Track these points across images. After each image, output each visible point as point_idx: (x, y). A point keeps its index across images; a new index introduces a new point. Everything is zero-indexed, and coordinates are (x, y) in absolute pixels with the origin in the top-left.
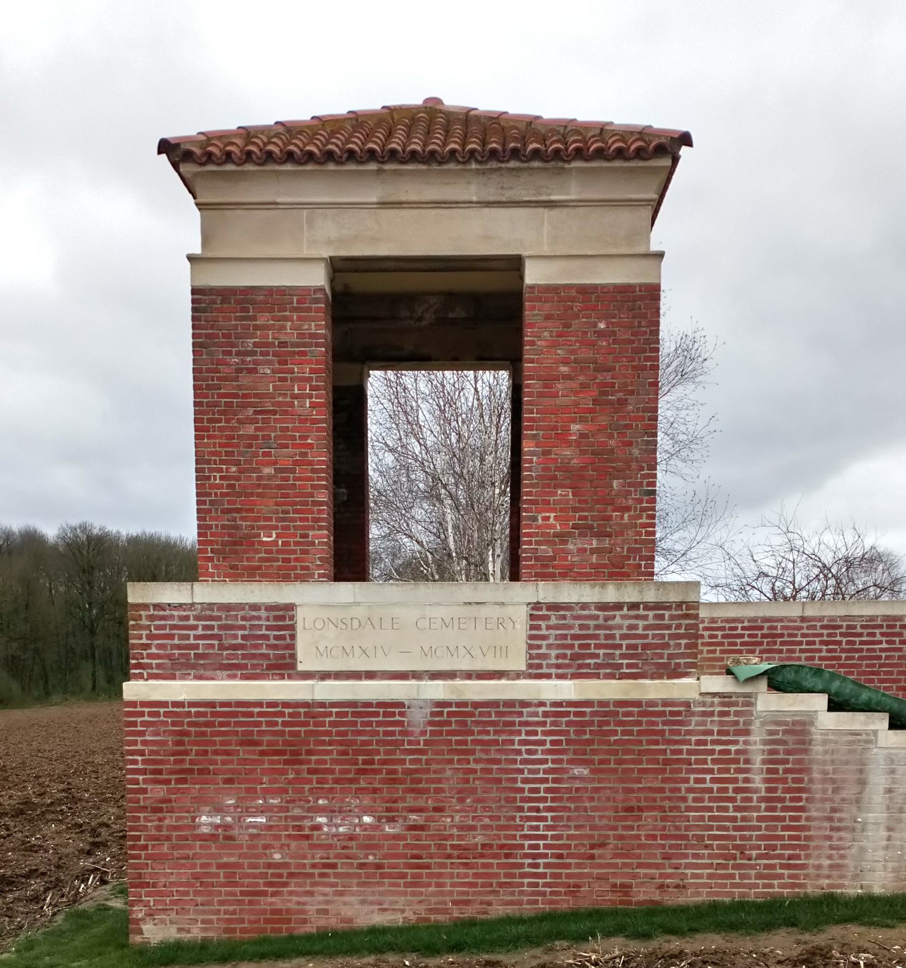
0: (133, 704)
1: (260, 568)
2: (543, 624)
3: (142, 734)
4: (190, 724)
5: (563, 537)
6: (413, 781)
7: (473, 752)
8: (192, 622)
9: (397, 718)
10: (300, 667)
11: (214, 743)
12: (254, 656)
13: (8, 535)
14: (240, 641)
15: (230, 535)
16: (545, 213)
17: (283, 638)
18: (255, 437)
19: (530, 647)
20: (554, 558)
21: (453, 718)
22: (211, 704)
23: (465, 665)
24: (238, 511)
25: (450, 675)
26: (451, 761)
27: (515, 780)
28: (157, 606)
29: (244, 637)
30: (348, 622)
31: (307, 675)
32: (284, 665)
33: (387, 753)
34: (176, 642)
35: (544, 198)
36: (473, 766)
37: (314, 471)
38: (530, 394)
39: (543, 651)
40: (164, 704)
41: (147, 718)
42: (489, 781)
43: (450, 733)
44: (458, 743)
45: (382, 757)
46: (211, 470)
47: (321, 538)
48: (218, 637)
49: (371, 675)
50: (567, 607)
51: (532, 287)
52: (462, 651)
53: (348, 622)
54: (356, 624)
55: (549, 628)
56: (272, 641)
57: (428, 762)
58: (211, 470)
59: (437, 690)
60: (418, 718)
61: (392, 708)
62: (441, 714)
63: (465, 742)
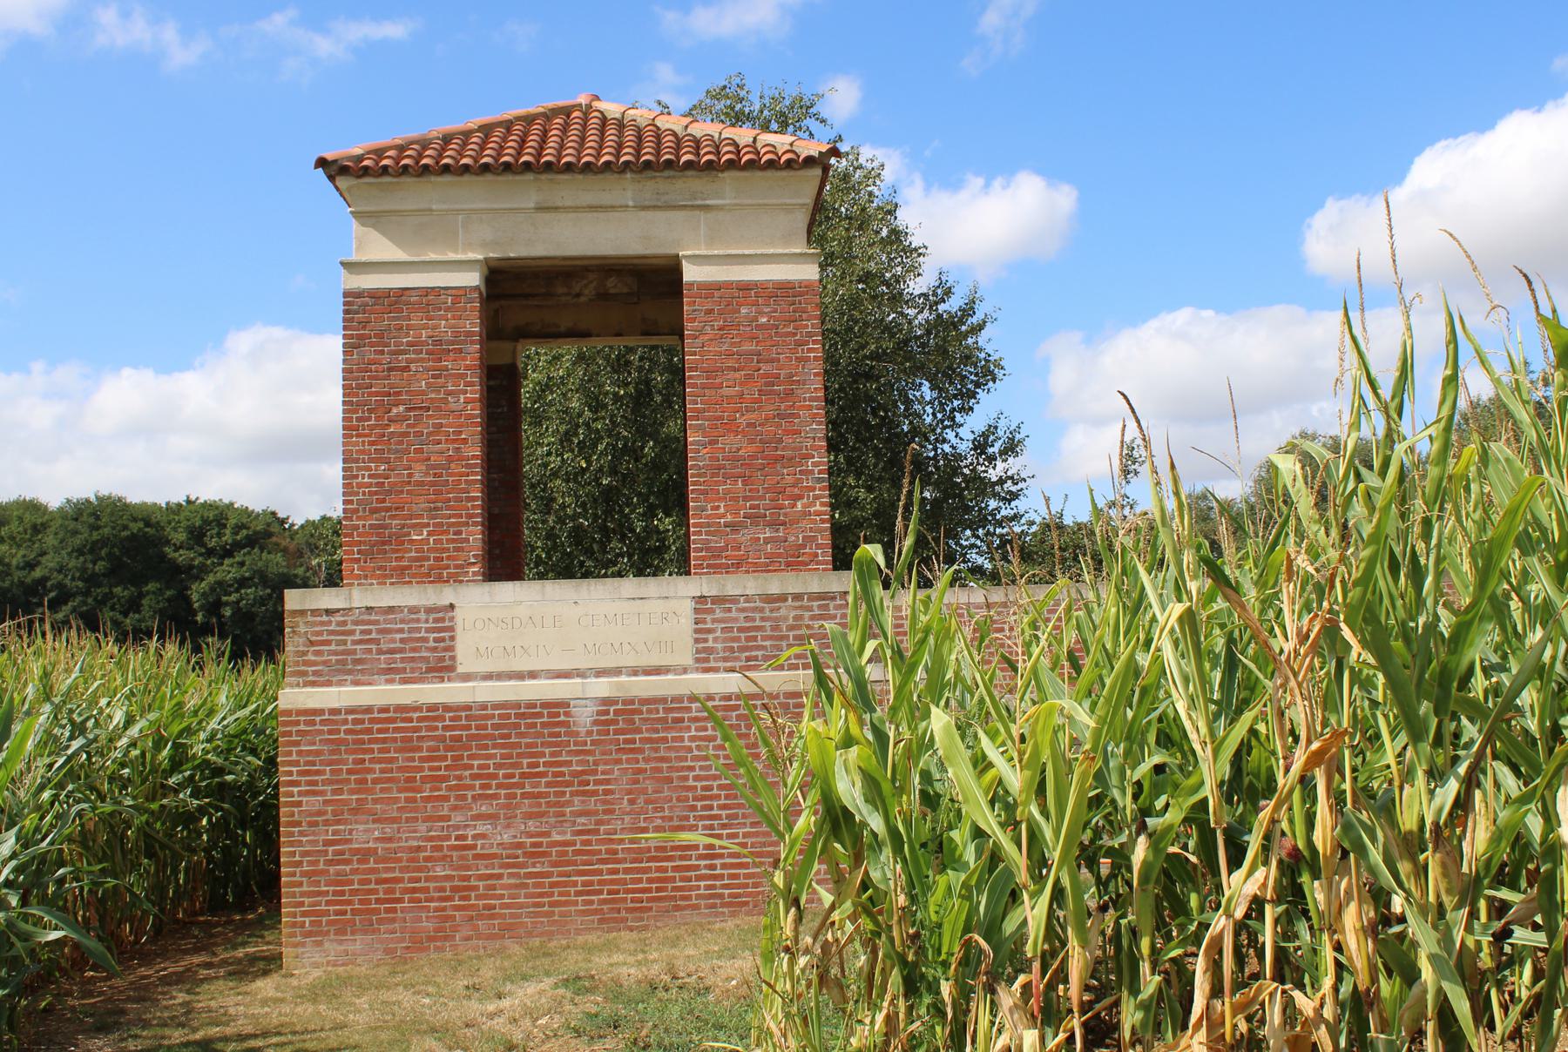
0: (288, 713)
1: (409, 567)
2: (709, 618)
3: (297, 743)
4: (347, 732)
5: (734, 527)
6: (581, 783)
7: (641, 751)
8: (349, 627)
9: (562, 718)
10: (460, 669)
11: (372, 751)
12: (413, 659)
13: (27, 519)
14: (398, 645)
15: (378, 535)
16: (702, 215)
17: (443, 640)
18: (407, 434)
19: (697, 641)
20: (725, 548)
21: (620, 717)
22: (369, 710)
23: (630, 661)
24: (388, 509)
25: (617, 671)
26: (618, 761)
27: (686, 778)
28: (315, 612)
29: (402, 641)
30: (509, 621)
31: (467, 677)
32: (443, 668)
33: (553, 754)
34: (333, 647)
35: (699, 202)
36: (642, 765)
37: (468, 466)
38: (694, 386)
39: (710, 644)
40: (320, 712)
41: (302, 727)
42: (658, 780)
43: (616, 732)
44: (626, 741)
45: (547, 759)
46: (359, 469)
47: (475, 536)
48: (377, 642)
49: (533, 675)
50: (733, 600)
51: (691, 284)
52: (626, 647)
53: (509, 621)
54: (517, 622)
55: (714, 621)
56: (432, 644)
57: (596, 763)
58: (359, 469)
59: (601, 687)
60: (584, 717)
61: (557, 707)
62: (607, 713)
63: (633, 741)
